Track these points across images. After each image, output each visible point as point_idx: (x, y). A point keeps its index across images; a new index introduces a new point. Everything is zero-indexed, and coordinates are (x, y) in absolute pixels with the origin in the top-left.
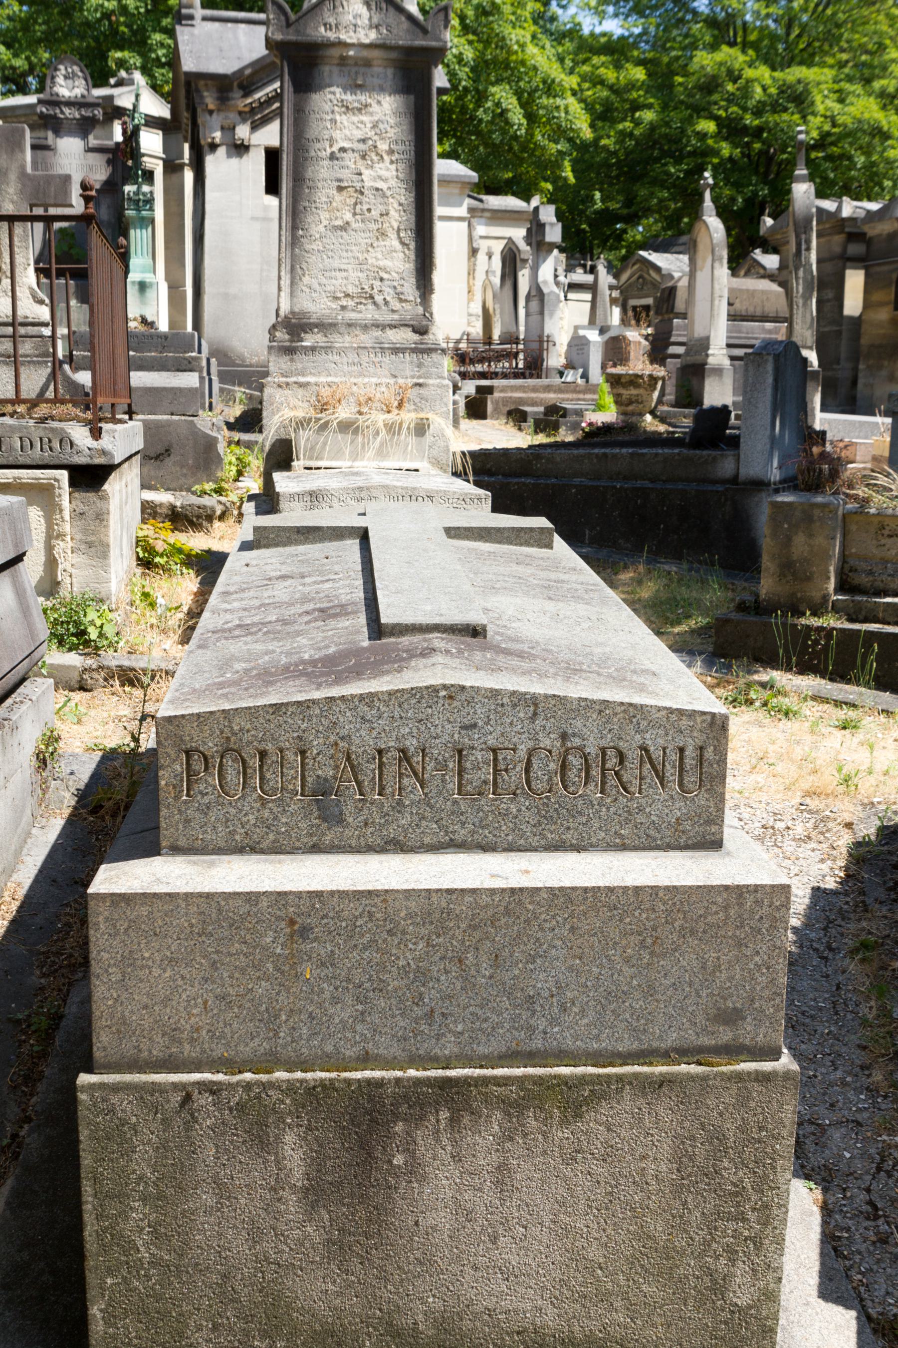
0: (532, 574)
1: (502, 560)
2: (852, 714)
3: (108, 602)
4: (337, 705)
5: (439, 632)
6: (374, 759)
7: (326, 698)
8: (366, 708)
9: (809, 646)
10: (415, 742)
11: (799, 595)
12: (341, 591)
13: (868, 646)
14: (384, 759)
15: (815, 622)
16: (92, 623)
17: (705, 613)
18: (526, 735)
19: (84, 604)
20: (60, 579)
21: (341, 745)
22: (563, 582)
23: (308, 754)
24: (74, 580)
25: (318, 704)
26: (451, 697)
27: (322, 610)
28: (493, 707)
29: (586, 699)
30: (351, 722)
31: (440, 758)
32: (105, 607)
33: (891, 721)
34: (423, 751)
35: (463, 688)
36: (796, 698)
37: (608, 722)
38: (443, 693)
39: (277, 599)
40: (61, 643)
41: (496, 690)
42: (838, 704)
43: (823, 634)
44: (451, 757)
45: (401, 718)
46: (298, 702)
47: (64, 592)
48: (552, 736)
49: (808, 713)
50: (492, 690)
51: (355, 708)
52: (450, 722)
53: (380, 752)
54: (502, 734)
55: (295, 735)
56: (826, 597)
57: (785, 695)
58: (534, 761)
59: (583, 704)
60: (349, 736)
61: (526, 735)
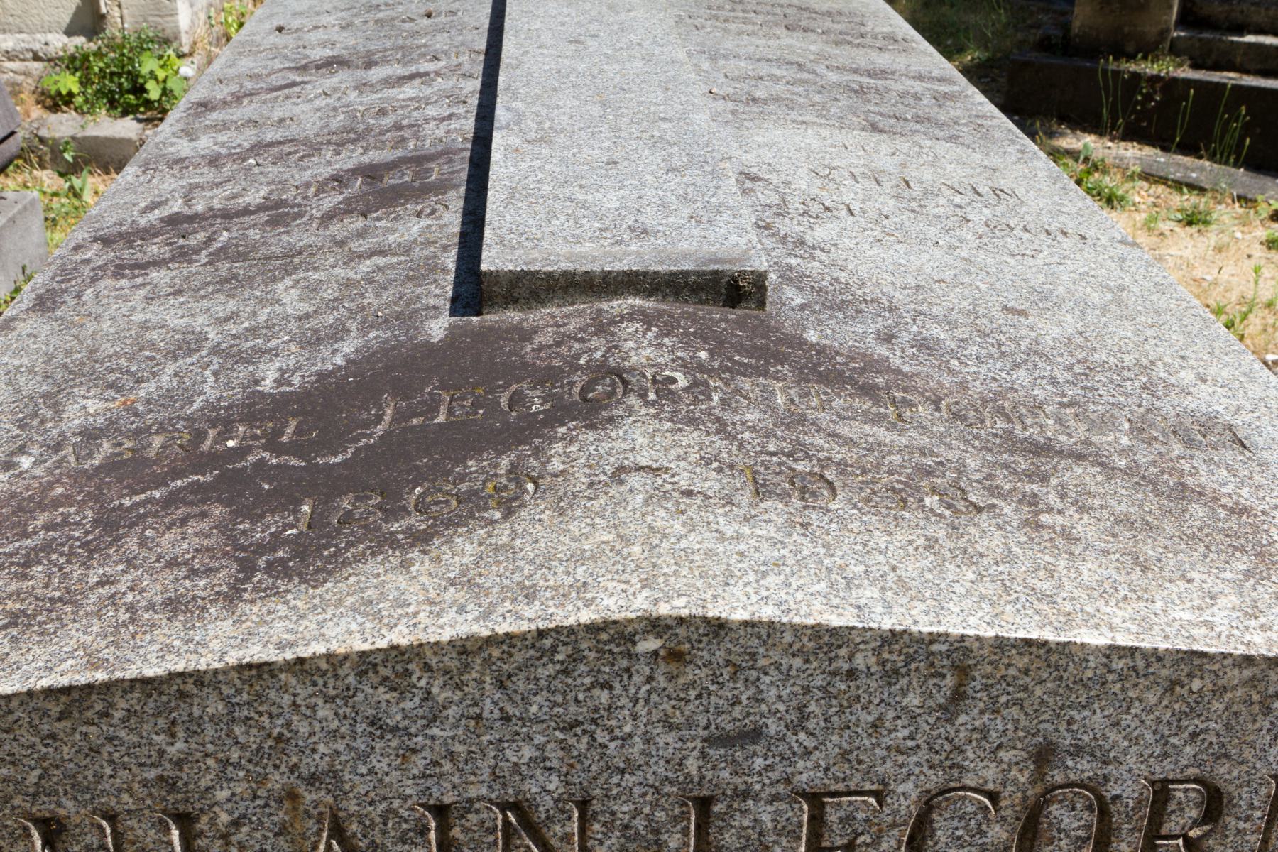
0: (822, 57)
1: (759, 19)
2: (1202, 202)
3: (175, 45)
4: (284, 688)
5: (637, 292)
6: (424, 831)
7: (241, 668)
8: (383, 694)
9: (1137, 102)
10: (554, 784)
11: (1126, 29)
12: (431, 111)
13: (1232, 108)
14: (456, 832)
15: (1149, 68)
16: (153, 75)
17: (983, 43)
18: (923, 755)
19: (142, 46)
20: (104, 10)
21: (309, 797)
22: (883, 74)
23: (203, 824)
24: (125, 12)
25: (216, 685)
26: (675, 656)
27: (371, 173)
28: (819, 681)
29: (1132, 651)
30: (334, 734)
31: (640, 823)
32: (170, 52)
33: (1252, 211)
34: (583, 805)
35: (719, 627)
36: (1119, 176)
37: (1192, 712)
38: (649, 644)
39: (293, 131)
40: (112, 104)
41: (834, 632)
42: (1178, 185)
43: (1158, 86)
44: (675, 820)
45: (506, 718)
46: (145, 682)
47: (112, 30)
48: (1005, 755)
49: (1137, 199)
50: (817, 631)
51: (348, 694)
52: (671, 727)
53: (441, 811)
54: (844, 755)
55: (152, 774)
56: (1164, 33)
57: (1105, 172)
58: (938, 820)
59: (1118, 664)
60: (335, 774)
61: (923, 755)
